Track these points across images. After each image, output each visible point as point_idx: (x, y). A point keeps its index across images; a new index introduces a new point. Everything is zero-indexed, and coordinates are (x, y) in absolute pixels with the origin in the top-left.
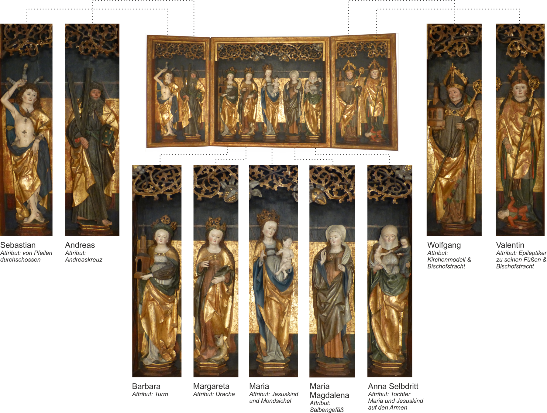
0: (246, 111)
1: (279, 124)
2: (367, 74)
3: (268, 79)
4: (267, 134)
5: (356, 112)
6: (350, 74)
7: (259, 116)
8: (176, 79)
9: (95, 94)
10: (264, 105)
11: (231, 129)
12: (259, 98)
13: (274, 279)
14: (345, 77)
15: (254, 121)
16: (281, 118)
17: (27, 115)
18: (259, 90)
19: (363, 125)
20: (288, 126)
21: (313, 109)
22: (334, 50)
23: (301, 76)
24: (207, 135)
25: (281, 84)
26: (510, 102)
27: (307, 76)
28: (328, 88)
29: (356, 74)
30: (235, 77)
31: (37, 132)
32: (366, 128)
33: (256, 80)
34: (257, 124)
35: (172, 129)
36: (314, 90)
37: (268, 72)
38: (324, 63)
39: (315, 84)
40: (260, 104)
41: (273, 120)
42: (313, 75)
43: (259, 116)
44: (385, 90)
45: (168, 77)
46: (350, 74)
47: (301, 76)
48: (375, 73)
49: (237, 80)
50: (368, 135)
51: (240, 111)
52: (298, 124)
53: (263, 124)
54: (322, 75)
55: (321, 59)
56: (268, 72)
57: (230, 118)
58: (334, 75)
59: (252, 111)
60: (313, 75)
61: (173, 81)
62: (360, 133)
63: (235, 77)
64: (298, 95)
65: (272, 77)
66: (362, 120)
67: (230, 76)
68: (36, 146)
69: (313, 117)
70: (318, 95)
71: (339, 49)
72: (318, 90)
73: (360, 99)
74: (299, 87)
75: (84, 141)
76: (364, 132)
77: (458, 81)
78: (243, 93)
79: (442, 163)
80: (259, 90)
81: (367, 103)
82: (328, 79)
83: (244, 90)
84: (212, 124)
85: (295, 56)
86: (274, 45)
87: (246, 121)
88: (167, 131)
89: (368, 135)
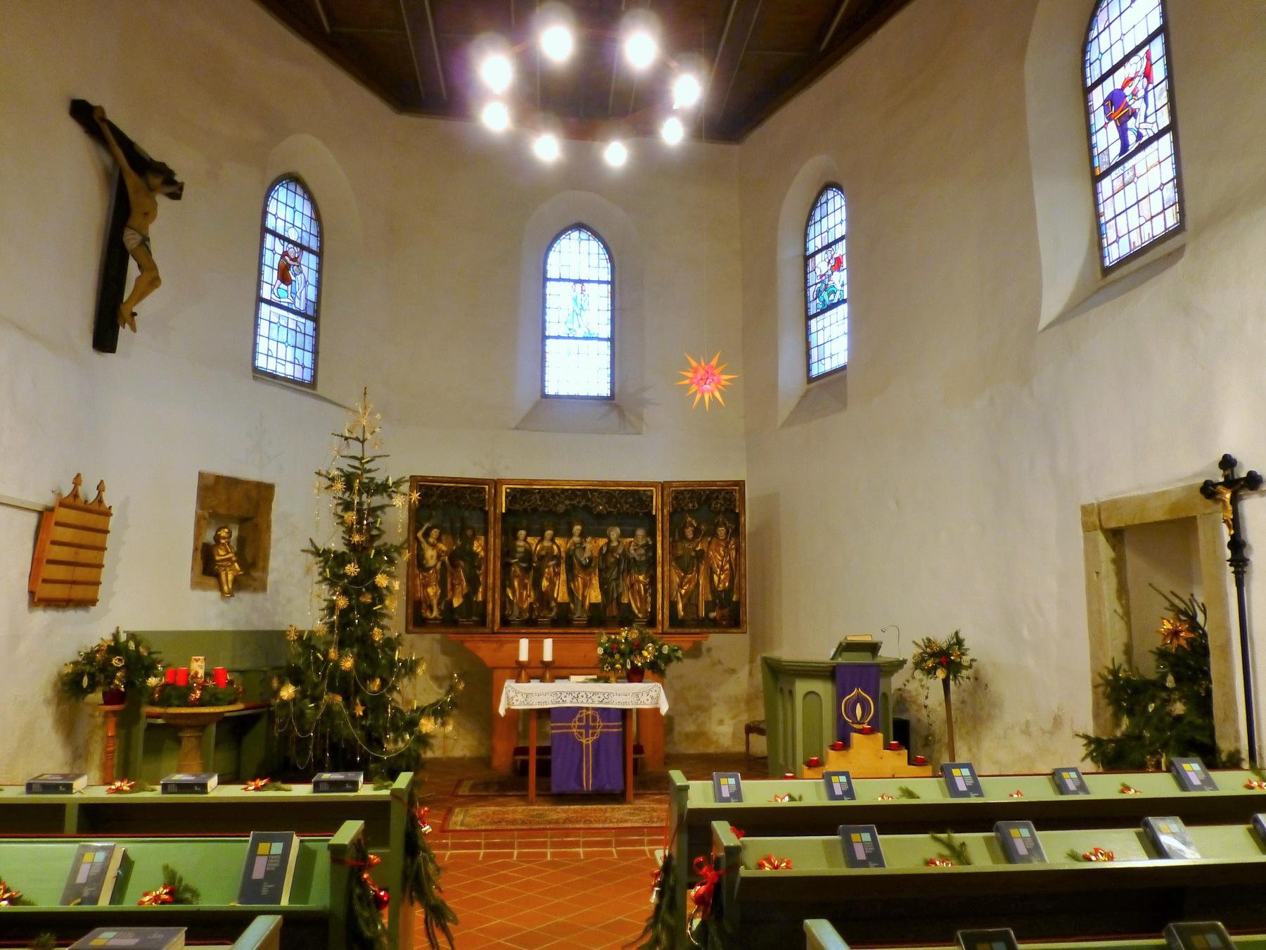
0: (545, 583)
1: (591, 604)
2: (714, 534)
3: (576, 539)
4: (575, 617)
5: (697, 584)
6: (689, 532)
7: (561, 594)
8: (443, 537)
9: (469, 532)
10: (571, 577)
11: (521, 611)
12: (563, 567)
13: (580, 562)
14: (683, 537)
15: (556, 600)
16: (595, 595)
17: (433, 546)
18: (563, 554)
19: (707, 603)
20: (605, 607)
21: (639, 581)
22: (668, 500)
23: (624, 535)
24: (489, 618)
25: (593, 546)
26: (715, 540)
27: (633, 535)
28: (659, 551)
29: (697, 532)
30: (528, 535)
31: (439, 557)
32: (710, 606)
33: (558, 541)
34: (559, 605)
35: (439, 610)
36: (640, 555)
37: (577, 529)
38: (654, 517)
39: (642, 546)
40: (563, 577)
41: (584, 597)
42: (640, 532)
43: (561, 594)
44: (733, 553)
45: (435, 533)
46: (689, 532)
47: (624, 535)
48: (721, 531)
49: (530, 539)
50: (713, 615)
51: (537, 584)
52: (619, 603)
53: (568, 604)
54: (651, 533)
55: (651, 512)
56: (577, 529)
57: (521, 594)
58: (667, 534)
59: (552, 584)
60: (640, 532)
61: (439, 539)
62: (702, 613)
63: (528, 535)
64: (618, 562)
65: (583, 535)
66: (704, 595)
67: (522, 533)
68: (439, 565)
69: (639, 591)
70: (647, 561)
71: (676, 498)
72: (646, 554)
73: (702, 568)
74: (620, 551)
75: (462, 563)
76: (707, 614)
77: (692, 525)
78: (541, 558)
79: (682, 579)
80: (563, 554)
81: (711, 572)
82: (659, 539)
83: (543, 553)
84: (498, 602)
85: (615, 507)
86: (585, 491)
87: (544, 599)
88: (432, 611)
89: (713, 615)
